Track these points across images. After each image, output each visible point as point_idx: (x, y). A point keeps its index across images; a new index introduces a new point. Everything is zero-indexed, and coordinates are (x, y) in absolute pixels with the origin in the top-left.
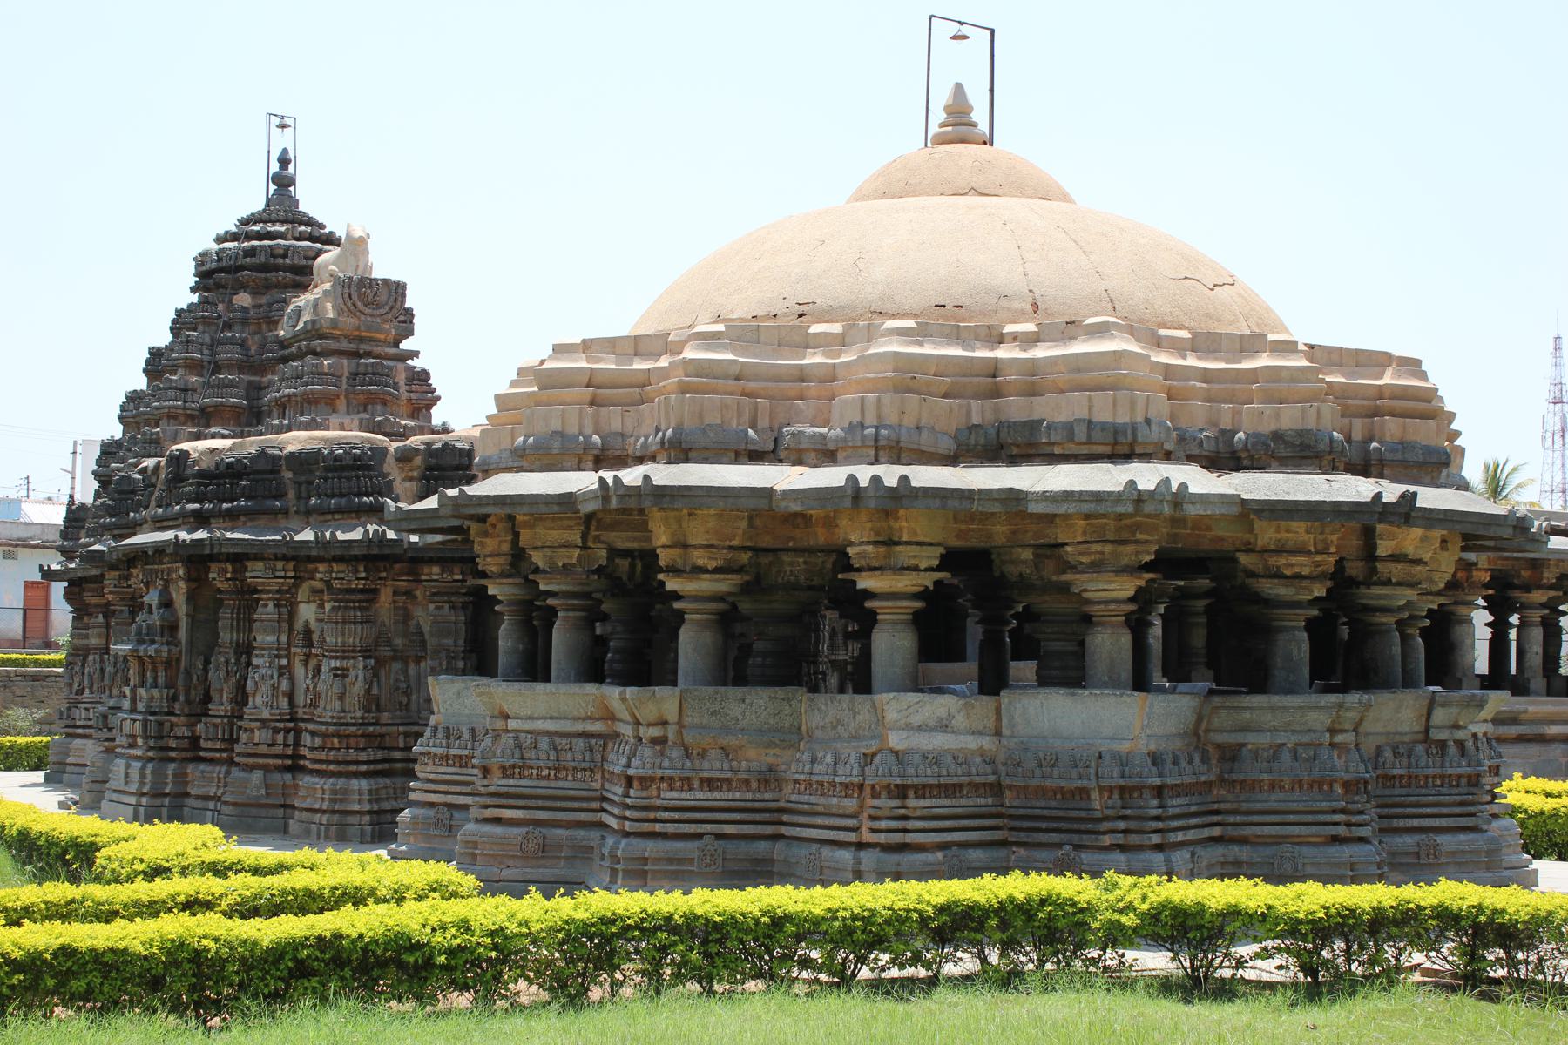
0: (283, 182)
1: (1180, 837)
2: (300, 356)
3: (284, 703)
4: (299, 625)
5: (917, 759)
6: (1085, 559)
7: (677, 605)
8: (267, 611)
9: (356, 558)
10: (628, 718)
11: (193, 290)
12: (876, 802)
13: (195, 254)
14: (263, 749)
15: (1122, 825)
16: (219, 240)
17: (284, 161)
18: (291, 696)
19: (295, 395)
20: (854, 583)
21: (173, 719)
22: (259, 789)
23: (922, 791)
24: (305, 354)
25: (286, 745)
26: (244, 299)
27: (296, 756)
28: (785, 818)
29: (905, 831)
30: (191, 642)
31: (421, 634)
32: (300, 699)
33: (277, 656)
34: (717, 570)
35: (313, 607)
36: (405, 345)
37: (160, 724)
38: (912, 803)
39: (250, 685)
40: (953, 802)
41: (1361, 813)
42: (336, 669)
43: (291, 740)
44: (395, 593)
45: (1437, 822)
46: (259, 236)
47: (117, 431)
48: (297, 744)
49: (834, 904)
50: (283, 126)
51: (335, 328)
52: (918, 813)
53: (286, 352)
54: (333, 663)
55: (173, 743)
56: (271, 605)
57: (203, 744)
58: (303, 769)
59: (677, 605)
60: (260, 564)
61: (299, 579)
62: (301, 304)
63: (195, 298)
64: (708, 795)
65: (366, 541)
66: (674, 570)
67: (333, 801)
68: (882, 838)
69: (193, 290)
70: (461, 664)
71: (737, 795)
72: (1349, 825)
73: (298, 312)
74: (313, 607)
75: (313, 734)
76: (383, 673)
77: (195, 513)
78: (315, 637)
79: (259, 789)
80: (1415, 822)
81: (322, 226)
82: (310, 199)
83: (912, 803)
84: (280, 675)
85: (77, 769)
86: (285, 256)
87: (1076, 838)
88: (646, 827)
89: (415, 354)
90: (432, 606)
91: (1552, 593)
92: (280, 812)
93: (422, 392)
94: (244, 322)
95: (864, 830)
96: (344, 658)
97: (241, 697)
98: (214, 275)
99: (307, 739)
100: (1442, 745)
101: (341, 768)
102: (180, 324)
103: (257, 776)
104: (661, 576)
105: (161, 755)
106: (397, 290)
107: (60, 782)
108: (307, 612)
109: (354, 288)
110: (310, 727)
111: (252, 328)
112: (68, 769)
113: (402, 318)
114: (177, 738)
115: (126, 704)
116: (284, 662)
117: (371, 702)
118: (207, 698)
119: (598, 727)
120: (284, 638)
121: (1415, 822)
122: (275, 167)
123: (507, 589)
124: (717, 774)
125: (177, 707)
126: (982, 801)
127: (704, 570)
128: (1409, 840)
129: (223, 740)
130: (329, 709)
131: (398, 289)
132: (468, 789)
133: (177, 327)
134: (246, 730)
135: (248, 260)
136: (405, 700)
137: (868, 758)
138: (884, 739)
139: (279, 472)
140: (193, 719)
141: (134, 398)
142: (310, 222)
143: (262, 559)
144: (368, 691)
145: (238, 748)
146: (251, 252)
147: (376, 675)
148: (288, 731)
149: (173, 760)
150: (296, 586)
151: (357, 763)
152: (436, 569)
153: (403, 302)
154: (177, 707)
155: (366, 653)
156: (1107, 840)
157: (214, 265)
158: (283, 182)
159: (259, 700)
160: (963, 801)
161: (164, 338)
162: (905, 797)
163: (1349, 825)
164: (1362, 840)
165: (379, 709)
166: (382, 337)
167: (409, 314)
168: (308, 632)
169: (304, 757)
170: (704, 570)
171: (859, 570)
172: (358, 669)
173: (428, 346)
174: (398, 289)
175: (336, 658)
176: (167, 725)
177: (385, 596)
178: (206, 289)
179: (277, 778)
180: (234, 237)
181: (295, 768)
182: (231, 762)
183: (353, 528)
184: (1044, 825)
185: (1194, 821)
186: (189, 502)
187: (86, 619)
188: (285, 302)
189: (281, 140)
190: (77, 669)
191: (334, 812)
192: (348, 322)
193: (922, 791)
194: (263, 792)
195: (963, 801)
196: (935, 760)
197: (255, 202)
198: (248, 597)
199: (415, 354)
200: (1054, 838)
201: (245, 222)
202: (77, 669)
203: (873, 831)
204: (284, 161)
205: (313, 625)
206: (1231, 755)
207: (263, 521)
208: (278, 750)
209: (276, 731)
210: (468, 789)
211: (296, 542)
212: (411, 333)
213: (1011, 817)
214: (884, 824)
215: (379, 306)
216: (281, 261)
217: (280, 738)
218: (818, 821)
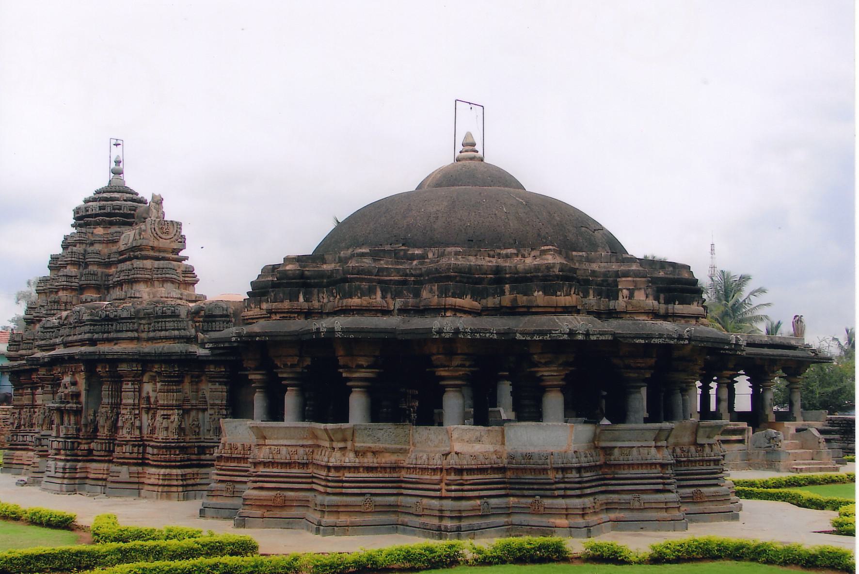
0: (117, 173)
1: (588, 491)
2: (130, 259)
3: (137, 432)
4: (144, 394)
5: (467, 456)
6: (543, 361)
7: (349, 384)
8: (128, 386)
9: (175, 361)
10: (327, 438)
11: (73, 226)
12: (449, 478)
13: (74, 208)
14: (127, 455)
15: (562, 486)
16: (86, 201)
18: (140, 428)
20: (435, 372)
23: (470, 471)
24: (133, 259)
25: (139, 453)
27: (144, 458)
28: (404, 485)
29: (462, 490)
30: (87, 403)
31: (205, 398)
32: (145, 431)
33: (133, 409)
34: (368, 367)
36: (182, 254)
37: (73, 443)
38: (331, 474)
39: (120, 424)
40: (355, 475)
41: (669, 478)
43: (141, 451)
44: (192, 377)
45: (701, 482)
46: (106, 199)
48: (144, 452)
50: (117, 145)
52: (469, 482)
54: (162, 412)
55: (80, 453)
57: (94, 452)
58: (148, 465)
59: (349, 384)
61: (144, 372)
63: (74, 230)
64: (366, 475)
66: (345, 367)
68: (453, 494)
69: (73, 226)
70: (225, 412)
71: (381, 475)
72: (664, 484)
75: (153, 447)
76: (186, 417)
77: (89, 340)
78: (152, 400)
80: (691, 483)
81: (137, 194)
82: (131, 181)
83: (466, 477)
84: (135, 418)
85: (18, 466)
87: (542, 492)
88: (338, 490)
89: (186, 258)
91: (732, 373)
92: (136, 486)
93: (188, 278)
95: (443, 491)
97: (115, 428)
98: (83, 218)
99: (149, 450)
100: (702, 445)
101: (168, 464)
102: (66, 244)
104: (341, 370)
105: (74, 457)
108: (148, 388)
110: (152, 444)
115: (54, 434)
116: (137, 412)
117: (181, 430)
118: (96, 430)
119: (310, 442)
120: (137, 401)
121: (691, 483)
122: (113, 165)
123: (258, 377)
124: (371, 465)
126: (496, 476)
127: (361, 367)
128: (689, 491)
129: (105, 451)
130: (161, 435)
131: (179, 225)
132: (246, 474)
133: (65, 245)
134: (118, 446)
135: (102, 211)
136: (197, 430)
137: (446, 455)
138: (452, 447)
142: (131, 192)
144: (180, 426)
145: (115, 454)
146: (101, 208)
147: (183, 418)
148: (139, 446)
150: (142, 374)
151: (175, 461)
155: (179, 407)
156: (556, 493)
158: (117, 173)
159: (125, 431)
160: (488, 477)
161: (59, 251)
162: (462, 475)
163: (664, 484)
164: (669, 491)
168: (148, 398)
169: (148, 459)
170: (361, 367)
171: (438, 367)
173: (194, 254)
174: (179, 225)
176: (76, 445)
177: (187, 380)
178: (80, 226)
179: (134, 469)
180: (94, 200)
181: (144, 463)
182: (110, 461)
184: (526, 487)
185: (594, 484)
189: (116, 152)
190: (16, 416)
193: (470, 471)
195: (488, 477)
196: (474, 457)
197: (102, 182)
198: (117, 380)
199: (186, 258)
200: (531, 492)
201: (98, 192)
202: (16, 416)
203: (448, 491)
204: (118, 162)
205: (152, 394)
206: (608, 451)
208: (135, 455)
209: (134, 446)
210: (246, 474)
211: (129, 351)
213: (510, 483)
214: (453, 487)
216: (117, 211)
217: (136, 449)
218: (420, 486)
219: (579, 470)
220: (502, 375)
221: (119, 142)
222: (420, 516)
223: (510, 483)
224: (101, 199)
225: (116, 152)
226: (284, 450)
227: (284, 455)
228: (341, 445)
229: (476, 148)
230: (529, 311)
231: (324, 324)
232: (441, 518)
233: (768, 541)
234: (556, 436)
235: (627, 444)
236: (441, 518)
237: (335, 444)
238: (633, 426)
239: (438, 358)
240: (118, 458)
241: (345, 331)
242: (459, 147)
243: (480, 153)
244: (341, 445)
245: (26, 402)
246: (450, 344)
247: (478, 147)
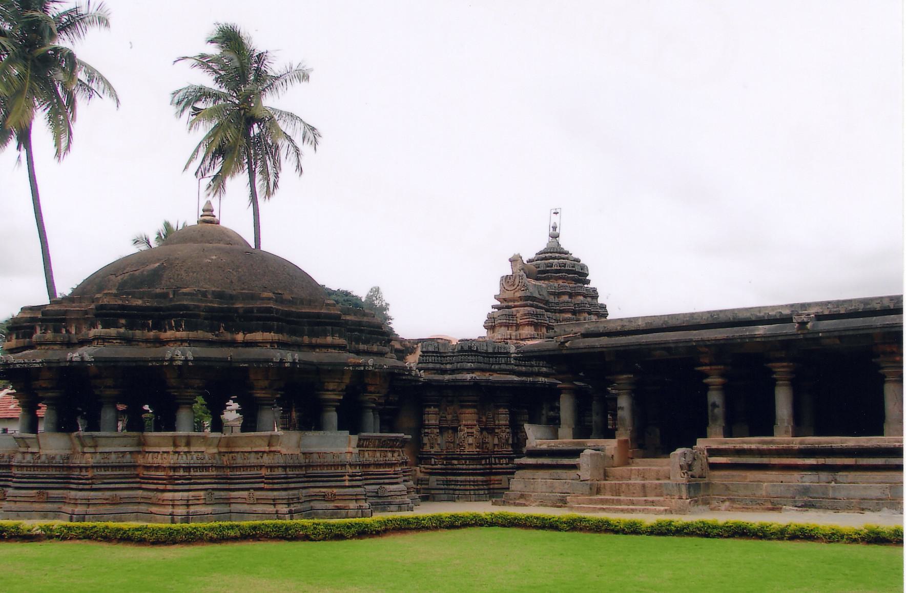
0: (555, 236)
82: (566, 243)
142: (567, 253)
189: (556, 219)
219: (285, 468)
220: (302, 397)
221: (558, 211)
222: (118, 504)
223: (267, 479)
224: (546, 259)
225: (556, 219)
226: (113, 456)
227: (207, 460)
228: (92, 450)
229: (214, 213)
230: (163, 343)
231: (75, 355)
232: (188, 505)
233: (805, 513)
234: (336, 444)
235: (107, 450)
236: (188, 505)
237: (86, 450)
238: (263, 433)
239: (173, 382)
240: (21, 467)
241: (97, 360)
242: (201, 213)
243: (217, 218)
244: (92, 450)
245: (433, 422)
246: (184, 370)
247: (215, 213)
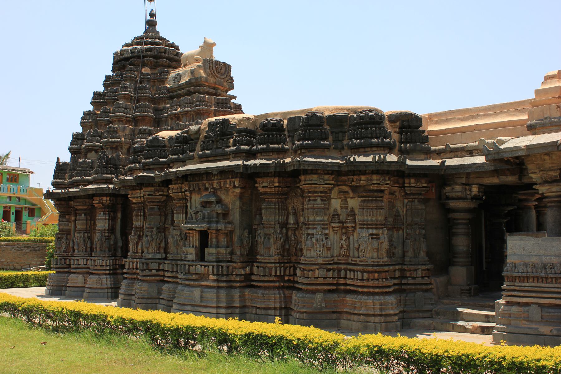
0: (151, 24)
14: (321, 280)
17: (152, 15)
19: (190, 111)
21: (235, 265)
22: (321, 303)
26: (146, 70)
35: (339, 201)
36: (230, 93)
42: (372, 234)
47: (79, 130)
49: (63, 306)
51: (206, 82)
53: (174, 95)
56: (319, 200)
60: (315, 177)
62: (181, 72)
65: (374, 162)
67: (381, 309)
73: (179, 77)
74: (339, 201)
79: (321, 303)
86: (165, 52)
89: (235, 97)
90: (406, 201)
94: (149, 80)
96: (376, 228)
98: (121, 62)
103: (319, 297)
106: (227, 68)
107: (64, 295)
109: (214, 65)
111: (151, 83)
112: (68, 288)
113: (230, 81)
114: (237, 275)
125: (235, 258)
129: (276, 276)
139: (322, 126)
140: (244, 264)
141: (87, 114)
143: (316, 174)
149: (235, 288)
152: (412, 181)
153: (230, 74)
154: (235, 258)
157: (130, 55)
158: (151, 24)
165: (289, 255)
166: (222, 88)
167: (232, 79)
172: (384, 234)
175: (372, 228)
176: (230, 268)
183: (369, 155)
186: (260, 145)
187: (67, 217)
188: (168, 73)
191: (381, 315)
192: (211, 80)
194: (324, 305)
197: (140, 30)
199: (235, 97)
207: (317, 152)
209: (328, 270)
212: (233, 88)
215: (222, 75)
